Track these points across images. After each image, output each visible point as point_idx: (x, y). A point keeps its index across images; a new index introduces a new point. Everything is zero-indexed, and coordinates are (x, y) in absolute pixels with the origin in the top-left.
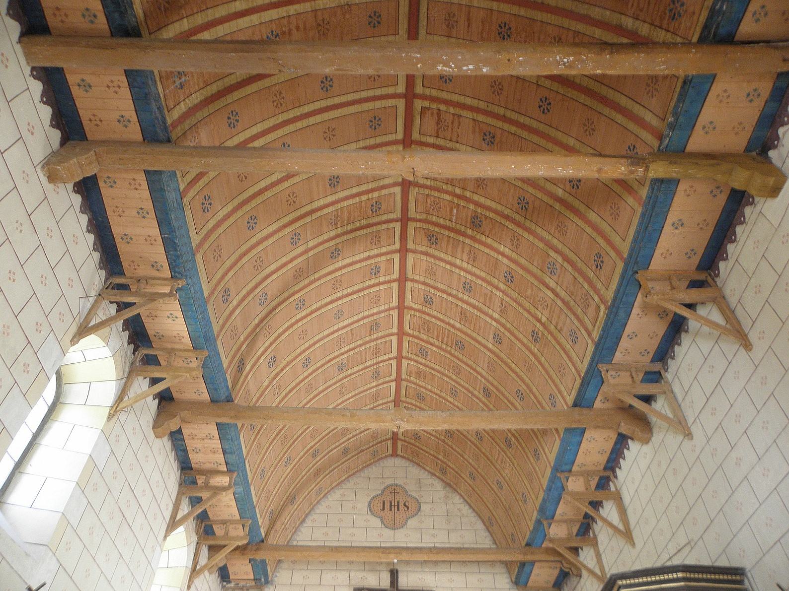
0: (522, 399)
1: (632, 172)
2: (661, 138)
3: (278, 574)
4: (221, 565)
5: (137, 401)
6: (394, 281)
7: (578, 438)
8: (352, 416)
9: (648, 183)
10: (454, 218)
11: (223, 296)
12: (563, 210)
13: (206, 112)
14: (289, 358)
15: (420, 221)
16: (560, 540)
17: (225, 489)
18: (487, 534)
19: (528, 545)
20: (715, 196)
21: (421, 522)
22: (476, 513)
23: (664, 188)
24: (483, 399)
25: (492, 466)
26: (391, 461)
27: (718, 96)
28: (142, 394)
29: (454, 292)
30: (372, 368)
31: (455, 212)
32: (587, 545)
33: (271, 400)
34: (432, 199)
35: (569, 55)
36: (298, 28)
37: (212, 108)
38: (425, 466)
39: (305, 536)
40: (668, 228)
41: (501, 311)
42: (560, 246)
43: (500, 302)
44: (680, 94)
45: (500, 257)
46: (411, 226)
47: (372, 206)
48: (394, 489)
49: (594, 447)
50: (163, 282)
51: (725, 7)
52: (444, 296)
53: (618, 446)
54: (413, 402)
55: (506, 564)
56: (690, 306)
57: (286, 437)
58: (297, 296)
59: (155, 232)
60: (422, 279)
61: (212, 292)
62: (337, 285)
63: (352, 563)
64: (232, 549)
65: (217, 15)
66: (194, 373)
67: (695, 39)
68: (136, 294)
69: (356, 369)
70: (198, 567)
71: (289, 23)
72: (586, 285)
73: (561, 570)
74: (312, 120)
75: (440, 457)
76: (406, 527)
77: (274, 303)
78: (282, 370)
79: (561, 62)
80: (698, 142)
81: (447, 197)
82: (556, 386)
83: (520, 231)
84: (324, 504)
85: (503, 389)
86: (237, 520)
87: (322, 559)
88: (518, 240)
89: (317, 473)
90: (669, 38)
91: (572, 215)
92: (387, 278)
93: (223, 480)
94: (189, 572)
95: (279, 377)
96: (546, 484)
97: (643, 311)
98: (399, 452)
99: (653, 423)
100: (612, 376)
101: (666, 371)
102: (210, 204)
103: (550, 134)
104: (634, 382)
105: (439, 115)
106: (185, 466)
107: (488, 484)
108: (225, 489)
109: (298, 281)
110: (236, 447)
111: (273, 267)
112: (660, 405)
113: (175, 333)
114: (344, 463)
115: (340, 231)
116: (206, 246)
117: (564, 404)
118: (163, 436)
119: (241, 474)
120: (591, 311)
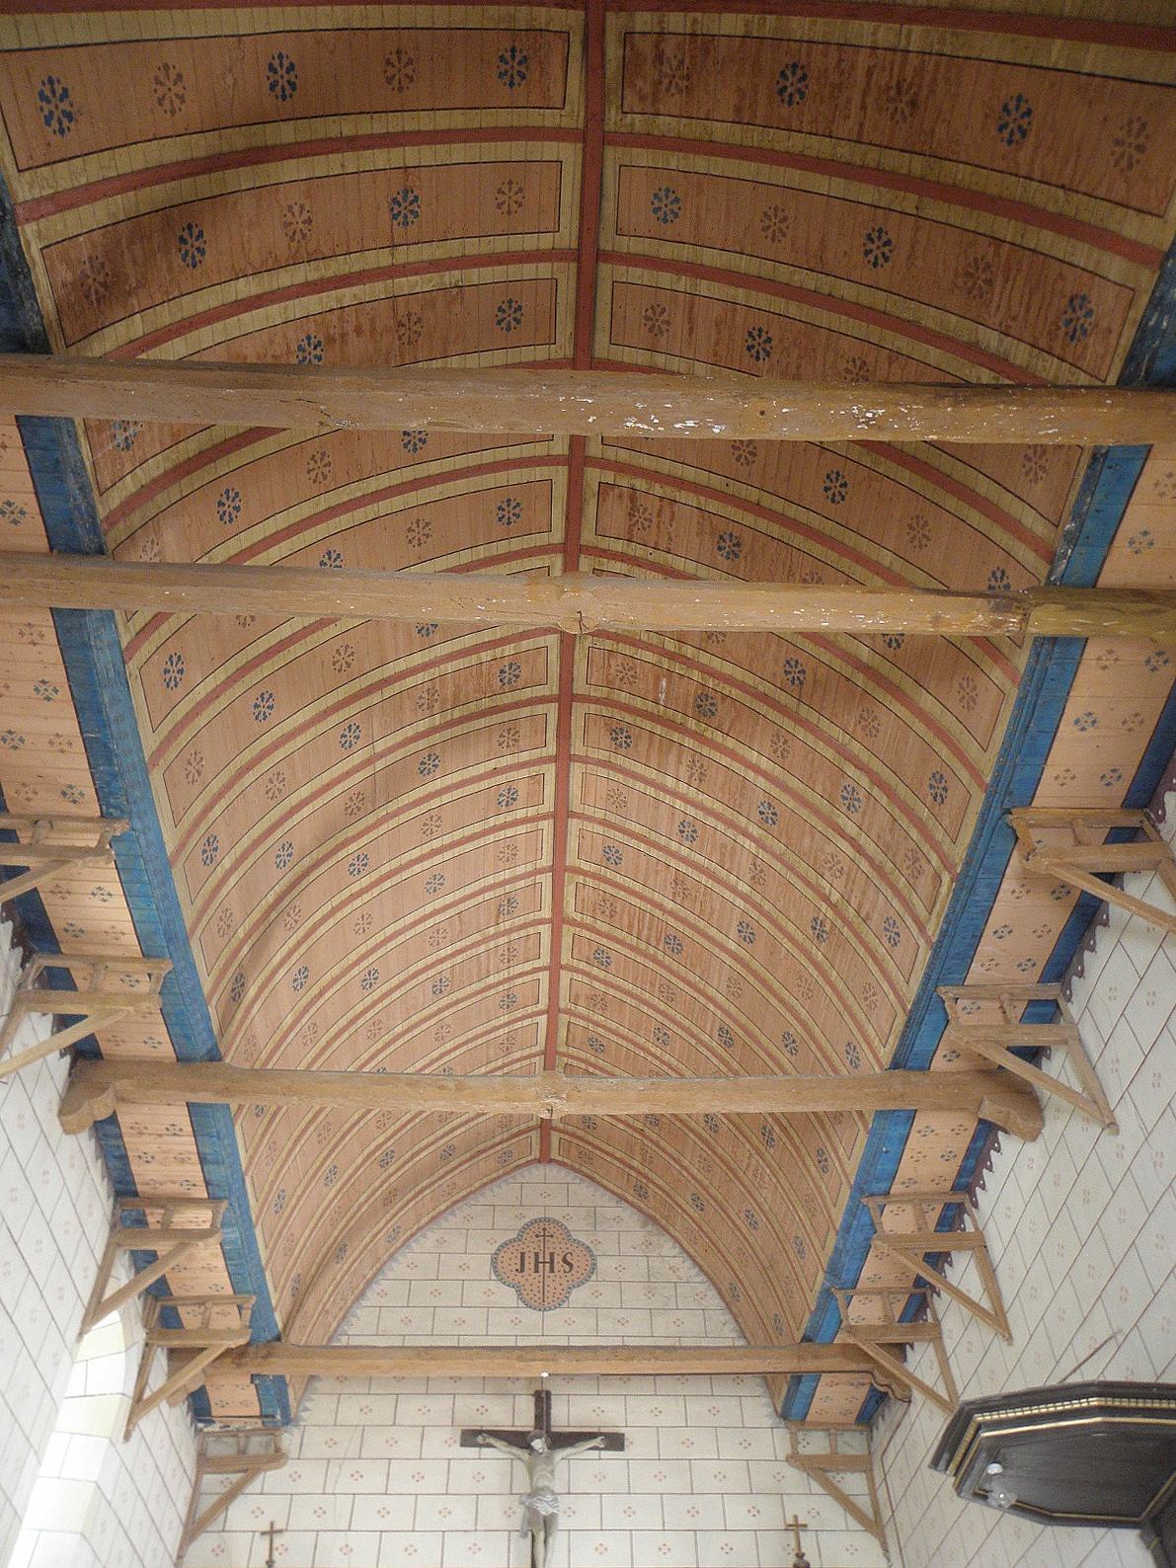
0: (794, 1052)
1: (997, 624)
2: (1051, 559)
3: (309, 1405)
4: (194, 1387)
5: (28, 1063)
6: (544, 817)
7: (902, 1130)
8: (460, 1087)
9: (1028, 644)
10: (662, 697)
11: (204, 851)
12: (870, 686)
13: (174, 493)
14: (336, 970)
15: (597, 701)
16: (871, 1329)
17: (203, 1235)
18: (728, 1317)
19: (806, 1339)
20: (1154, 669)
21: (597, 1294)
22: (706, 1274)
23: (1057, 658)
24: (719, 1050)
25: (737, 1183)
26: (537, 1173)
27: (1157, 484)
28: (38, 1047)
29: (663, 841)
30: (501, 988)
31: (664, 684)
32: (922, 1340)
33: (297, 1056)
34: (620, 659)
35: (876, 405)
36: (358, 330)
37: (187, 484)
38: (605, 1182)
39: (364, 1327)
40: (1066, 730)
41: (753, 878)
42: (865, 756)
43: (750, 861)
44: (1087, 479)
45: (751, 775)
46: (579, 710)
47: (502, 672)
48: (544, 1229)
49: (933, 1146)
50: (80, 825)
51: (1165, 324)
52: (643, 847)
53: (979, 1144)
54: (583, 1055)
55: (767, 1379)
56: (1111, 878)
57: (327, 1127)
58: (352, 847)
59: (70, 726)
60: (600, 814)
61: (183, 845)
62: (431, 825)
63: (455, 1379)
64: (219, 1352)
65: (202, 307)
66: (144, 1006)
67: (1112, 380)
68: (31, 849)
69: (468, 990)
70: (147, 1394)
71: (341, 319)
72: (914, 833)
73: (873, 1389)
74: (384, 506)
75: (635, 1164)
76: (565, 1305)
77: (307, 862)
78: (321, 994)
79: (854, 417)
80: (1120, 568)
81: (650, 657)
82: (860, 1028)
83: (789, 724)
84: (405, 1258)
85: (757, 1032)
86: (229, 1297)
87: (397, 1373)
88: (785, 742)
89: (389, 1199)
90: (1065, 374)
91: (889, 697)
92: (531, 812)
93: (199, 1218)
94: (128, 1403)
95: (314, 1009)
96: (840, 1220)
97: (1023, 886)
98: (554, 1155)
99: (1045, 1101)
100: (965, 1008)
101: (1069, 999)
102: (181, 671)
103: (846, 541)
104: (1007, 1021)
105: (633, 499)
106: (123, 1188)
107: (730, 1218)
108: (203, 1235)
109: (354, 818)
110: (225, 1148)
111: (305, 792)
112: (1057, 1066)
113: (106, 926)
114: (443, 1177)
115: (437, 720)
116: (171, 754)
117: (873, 1062)
118: (81, 1128)
119: (236, 1205)
120: (925, 883)
